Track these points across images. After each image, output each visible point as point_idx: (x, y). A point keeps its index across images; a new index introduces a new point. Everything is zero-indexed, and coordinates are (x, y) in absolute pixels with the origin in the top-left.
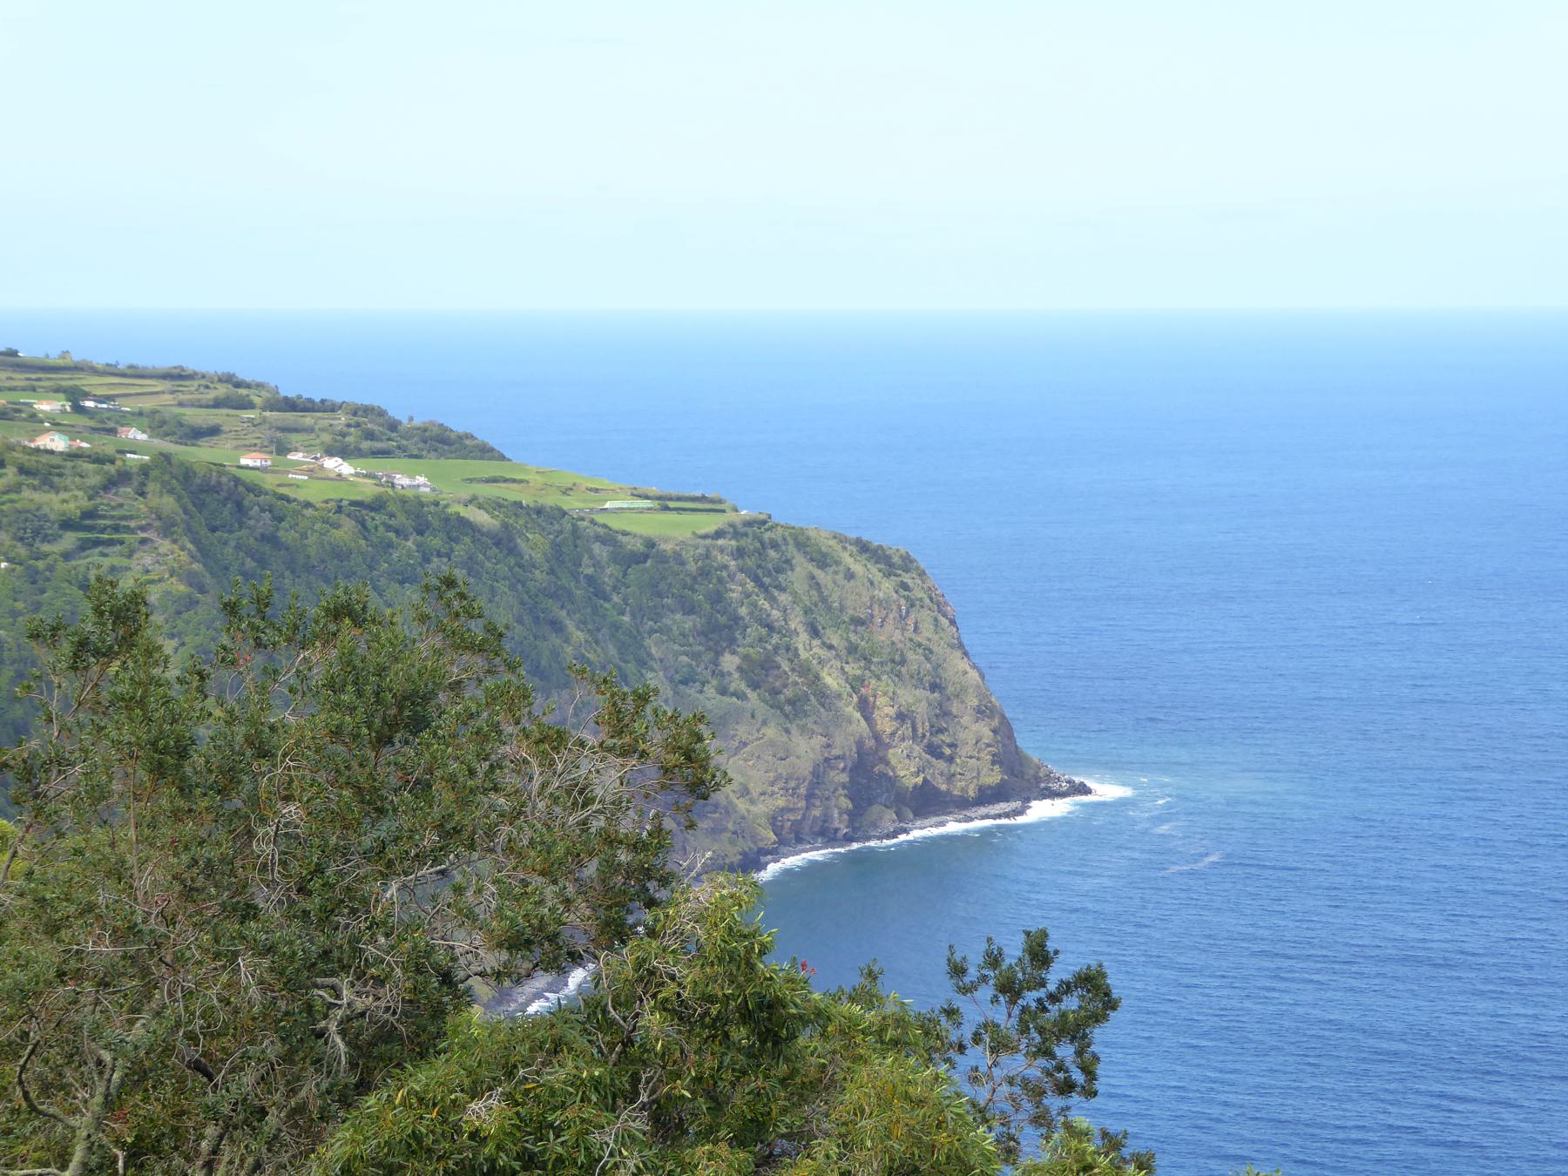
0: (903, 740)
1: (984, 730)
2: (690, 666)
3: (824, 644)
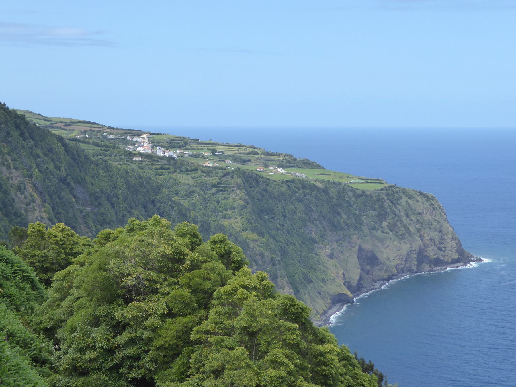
1: (454, 243)
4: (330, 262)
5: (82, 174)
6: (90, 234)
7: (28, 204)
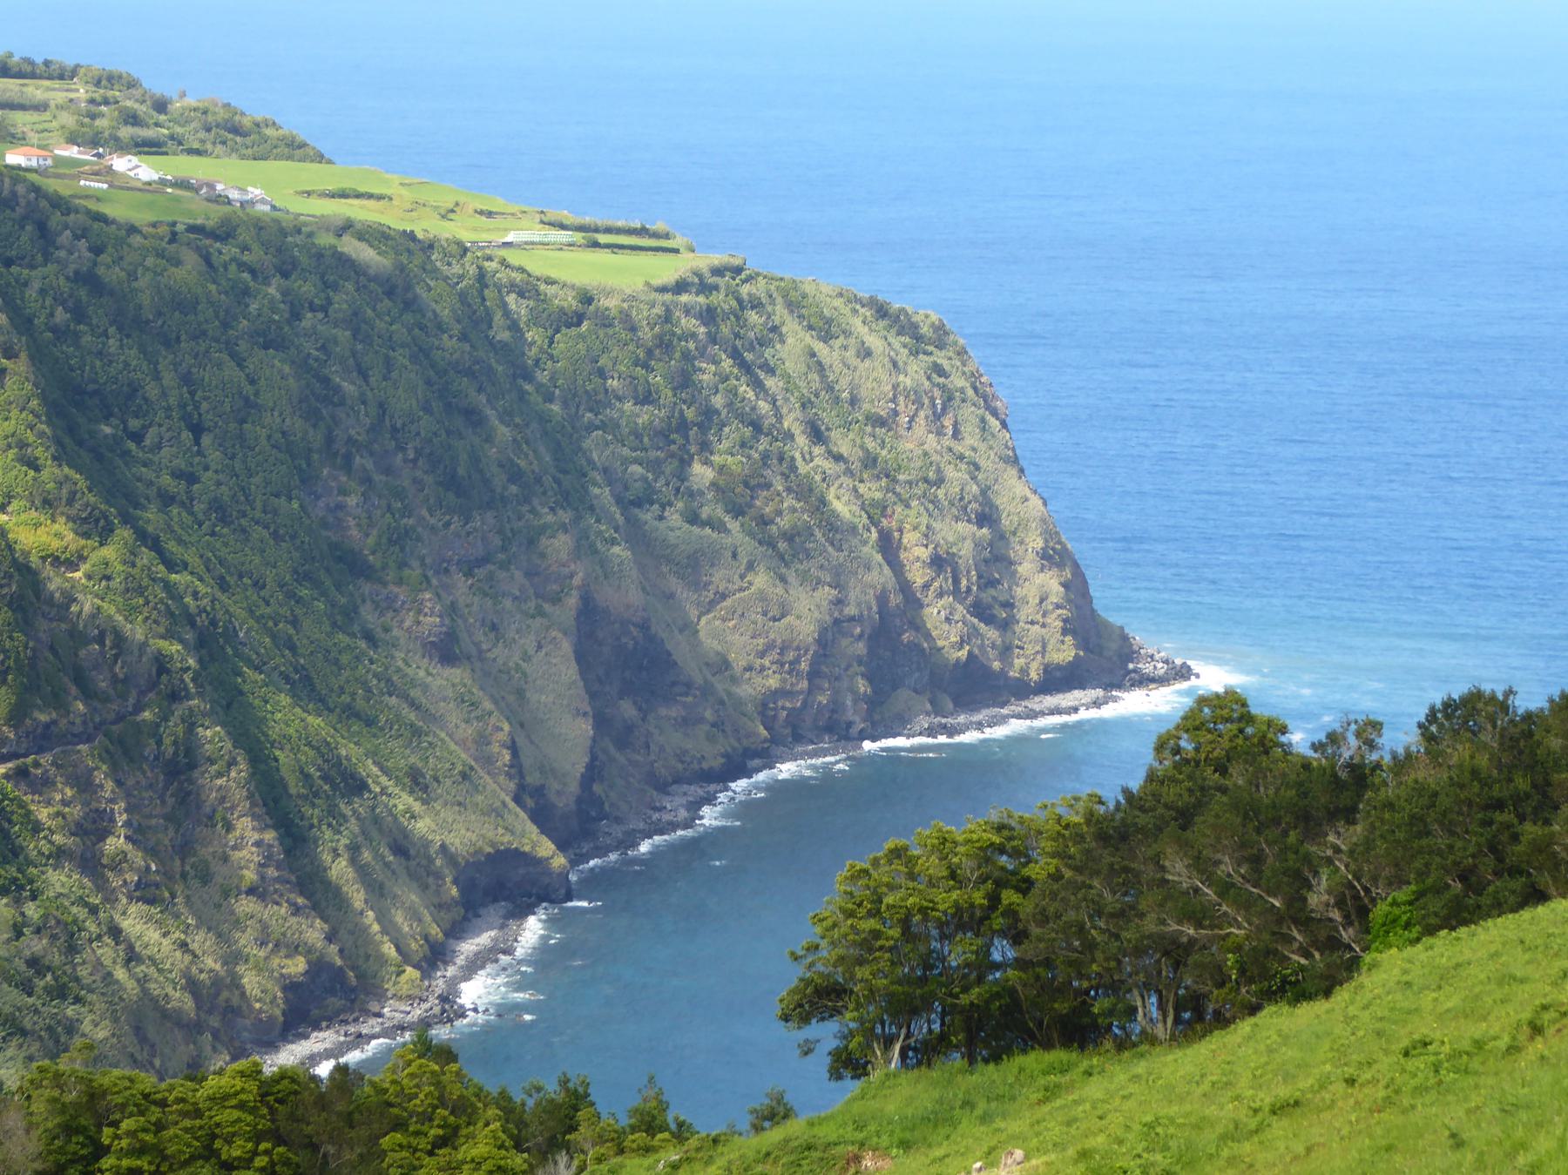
0: (940, 595)
1: (1052, 583)
2: (645, 479)
3: (829, 452)
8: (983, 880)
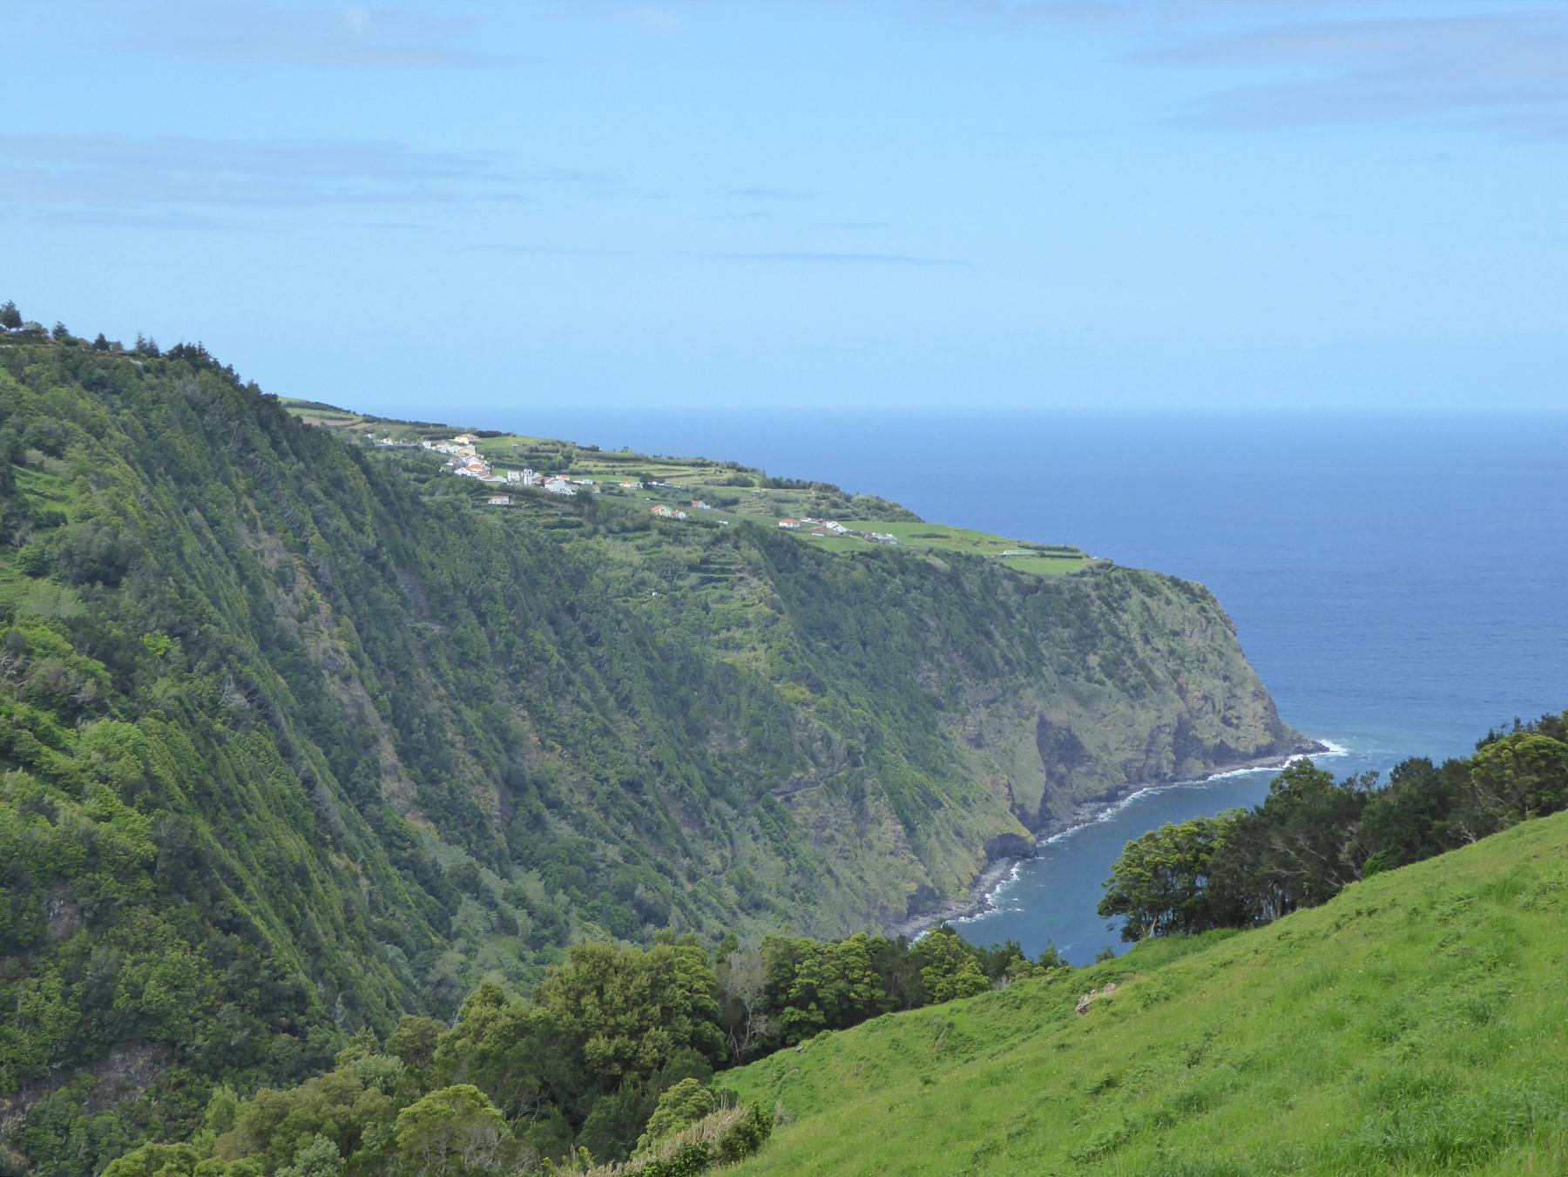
1: (1258, 707)
4: (973, 756)
5: (408, 541)
6: (442, 691)
7: (301, 619)
8: (1190, 849)
